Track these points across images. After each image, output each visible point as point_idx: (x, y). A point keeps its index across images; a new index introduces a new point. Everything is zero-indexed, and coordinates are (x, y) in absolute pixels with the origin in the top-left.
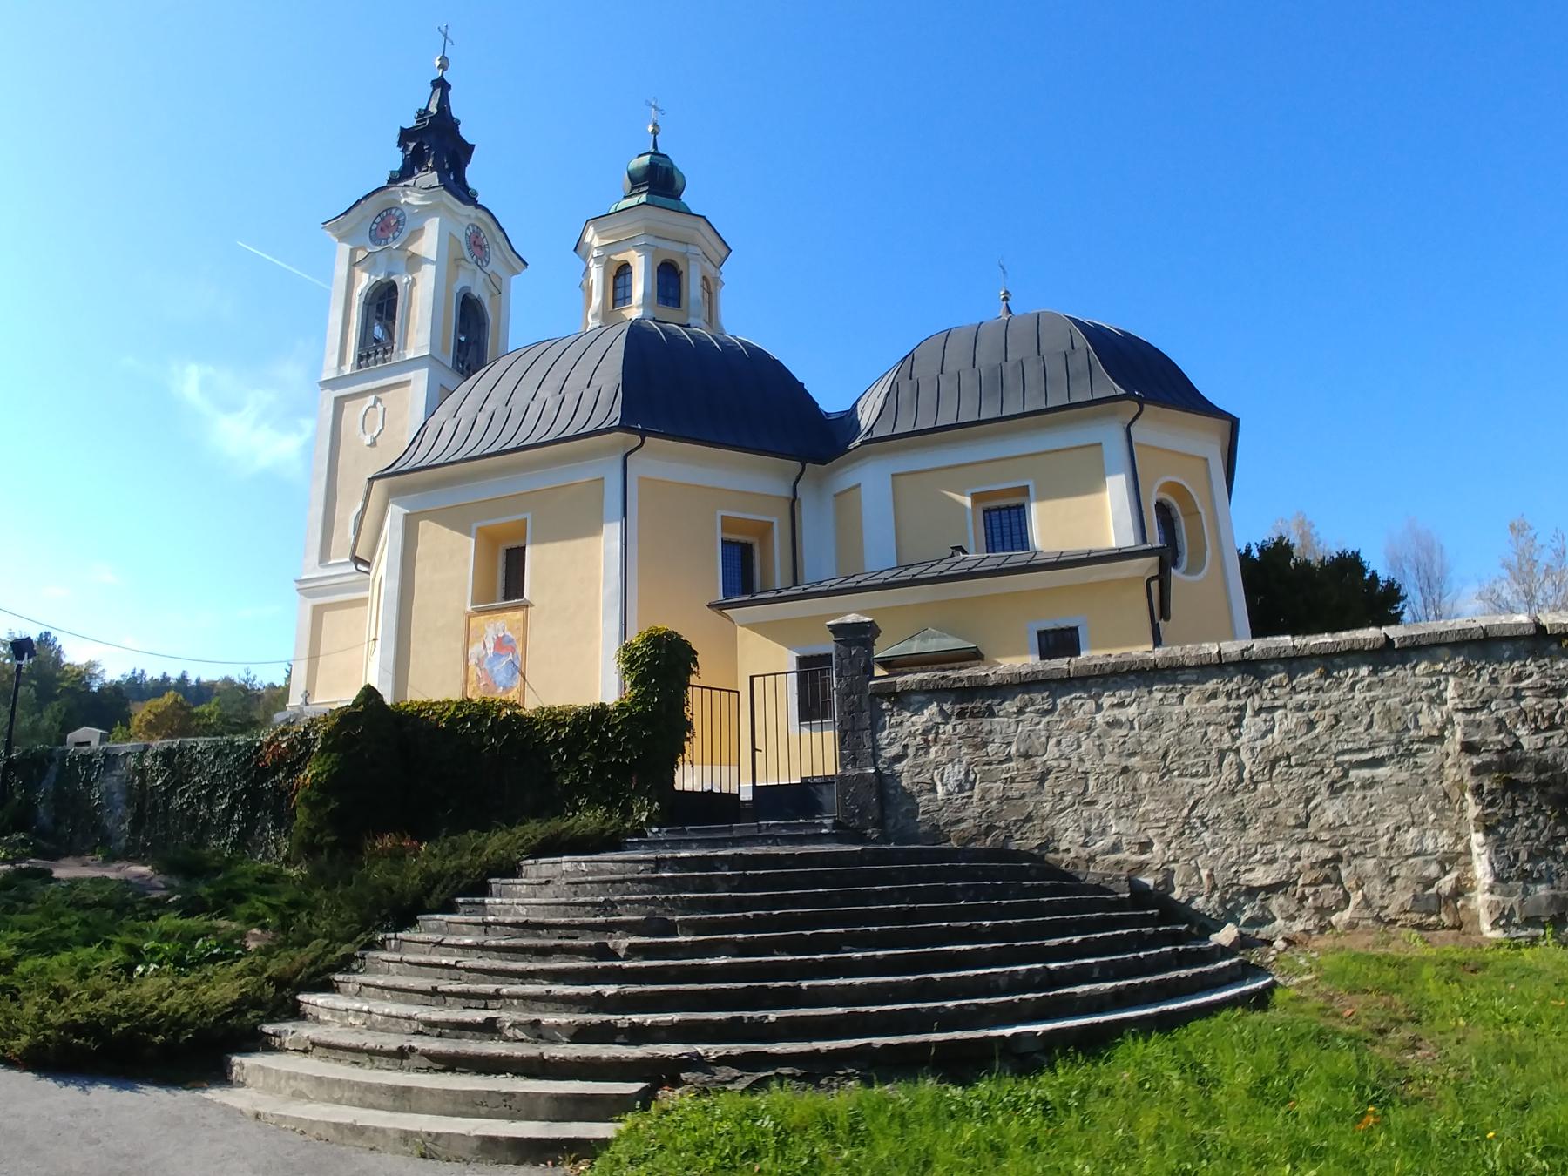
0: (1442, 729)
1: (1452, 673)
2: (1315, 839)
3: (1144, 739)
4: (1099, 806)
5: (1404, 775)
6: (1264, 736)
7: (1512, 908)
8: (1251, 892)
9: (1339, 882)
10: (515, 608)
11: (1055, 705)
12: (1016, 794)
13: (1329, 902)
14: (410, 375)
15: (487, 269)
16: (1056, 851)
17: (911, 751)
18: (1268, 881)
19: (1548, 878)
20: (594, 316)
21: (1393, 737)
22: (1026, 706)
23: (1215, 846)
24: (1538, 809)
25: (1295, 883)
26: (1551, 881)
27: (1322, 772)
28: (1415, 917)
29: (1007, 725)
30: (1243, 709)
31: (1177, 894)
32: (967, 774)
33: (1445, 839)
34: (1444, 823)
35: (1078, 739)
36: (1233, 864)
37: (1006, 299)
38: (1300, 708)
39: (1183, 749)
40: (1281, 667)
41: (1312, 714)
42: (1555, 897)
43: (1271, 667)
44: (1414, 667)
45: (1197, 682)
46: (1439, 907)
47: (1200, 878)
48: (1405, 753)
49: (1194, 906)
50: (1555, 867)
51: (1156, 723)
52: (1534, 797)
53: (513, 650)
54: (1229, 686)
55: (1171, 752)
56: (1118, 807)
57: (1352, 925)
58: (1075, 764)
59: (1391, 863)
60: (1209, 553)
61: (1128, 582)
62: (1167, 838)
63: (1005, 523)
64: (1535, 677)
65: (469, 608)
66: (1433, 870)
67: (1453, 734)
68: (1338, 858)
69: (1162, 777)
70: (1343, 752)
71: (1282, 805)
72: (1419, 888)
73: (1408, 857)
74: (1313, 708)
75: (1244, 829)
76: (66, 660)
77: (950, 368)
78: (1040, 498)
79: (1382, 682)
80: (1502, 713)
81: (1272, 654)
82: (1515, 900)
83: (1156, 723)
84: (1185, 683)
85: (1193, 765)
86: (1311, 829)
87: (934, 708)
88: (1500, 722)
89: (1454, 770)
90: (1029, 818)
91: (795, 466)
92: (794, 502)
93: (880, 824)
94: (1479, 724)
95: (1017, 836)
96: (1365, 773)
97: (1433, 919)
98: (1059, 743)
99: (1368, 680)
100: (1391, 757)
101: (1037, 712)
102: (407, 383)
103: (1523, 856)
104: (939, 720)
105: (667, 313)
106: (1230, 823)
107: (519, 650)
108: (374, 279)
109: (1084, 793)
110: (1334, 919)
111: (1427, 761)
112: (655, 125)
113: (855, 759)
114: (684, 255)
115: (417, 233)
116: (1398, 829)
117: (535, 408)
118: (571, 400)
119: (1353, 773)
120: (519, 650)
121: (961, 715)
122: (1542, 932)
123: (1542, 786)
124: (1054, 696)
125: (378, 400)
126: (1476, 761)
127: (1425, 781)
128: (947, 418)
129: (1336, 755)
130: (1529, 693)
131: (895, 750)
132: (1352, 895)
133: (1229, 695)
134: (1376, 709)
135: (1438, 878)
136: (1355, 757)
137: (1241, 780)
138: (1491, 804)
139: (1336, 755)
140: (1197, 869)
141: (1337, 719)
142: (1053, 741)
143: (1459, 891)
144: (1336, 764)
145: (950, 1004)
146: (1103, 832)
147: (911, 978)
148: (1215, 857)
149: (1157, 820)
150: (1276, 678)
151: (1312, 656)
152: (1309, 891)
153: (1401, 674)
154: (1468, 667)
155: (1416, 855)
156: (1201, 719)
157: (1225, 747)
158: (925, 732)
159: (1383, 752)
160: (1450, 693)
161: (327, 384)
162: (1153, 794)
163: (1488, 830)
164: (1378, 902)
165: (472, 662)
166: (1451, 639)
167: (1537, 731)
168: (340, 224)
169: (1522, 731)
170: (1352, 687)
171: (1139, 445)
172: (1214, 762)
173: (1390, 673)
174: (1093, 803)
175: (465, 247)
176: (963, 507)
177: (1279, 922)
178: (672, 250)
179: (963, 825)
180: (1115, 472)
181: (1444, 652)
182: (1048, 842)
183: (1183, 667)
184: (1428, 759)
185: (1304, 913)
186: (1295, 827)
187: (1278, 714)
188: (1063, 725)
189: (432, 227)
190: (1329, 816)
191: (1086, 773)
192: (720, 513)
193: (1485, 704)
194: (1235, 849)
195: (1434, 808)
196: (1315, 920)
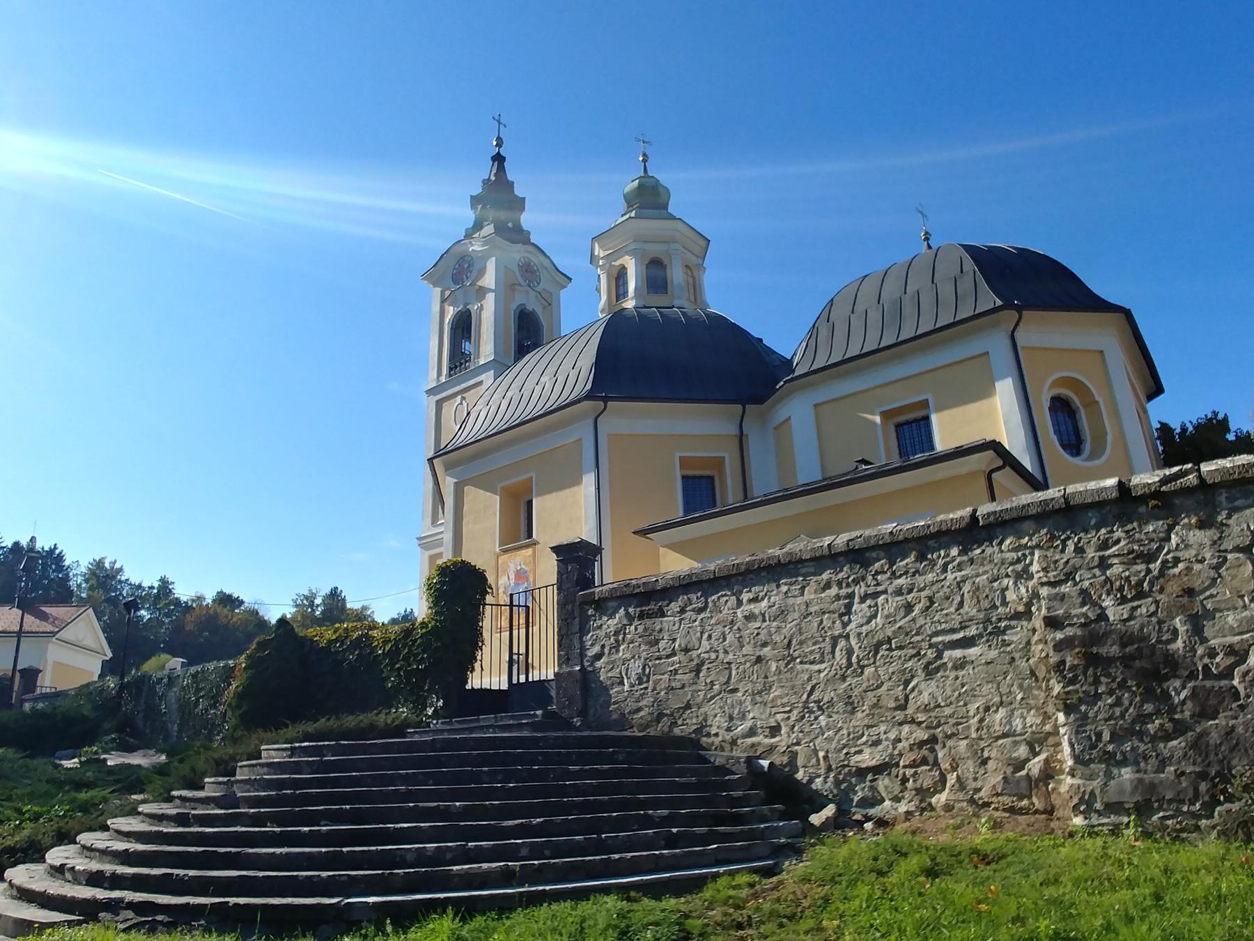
0: (1029, 605)
1: (1038, 546)
2: (913, 721)
3: (773, 630)
4: (739, 694)
5: (993, 654)
6: (868, 622)
7: (1092, 793)
8: (861, 773)
9: (936, 763)
10: (527, 546)
11: (706, 602)
12: (678, 685)
13: (927, 783)
14: (483, 377)
15: (539, 289)
16: (708, 735)
17: (606, 650)
18: (873, 763)
19: (1133, 760)
20: (602, 311)
21: (981, 616)
22: (686, 606)
23: (829, 729)
24: (1123, 685)
25: (897, 765)
26: (1137, 763)
27: (918, 653)
28: (1006, 800)
29: (675, 624)
30: (851, 596)
31: (800, 775)
32: (644, 669)
33: (1032, 719)
34: (1032, 702)
35: (723, 634)
36: (845, 746)
37: (927, 239)
38: (899, 592)
39: (803, 637)
40: (882, 554)
41: (909, 598)
42: (1140, 781)
43: (874, 555)
44: (1001, 543)
45: (815, 574)
46: (1027, 788)
47: (818, 760)
48: (994, 631)
49: (813, 786)
50: (1142, 747)
51: (782, 613)
52: (1118, 672)
53: (527, 580)
54: (840, 576)
55: (794, 642)
56: (753, 694)
57: (948, 808)
58: (721, 656)
59: (983, 744)
60: (1110, 438)
61: (971, 476)
62: (791, 722)
63: (912, 432)
64: (1123, 543)
66: (1023, 751)
67: (1039, 609)
68: (933, 740)
69: (787, 665)
70: (937, 634)
71: (884, 688)
72: (1009, 770)
73: (998, 738)
74: (910, 591)
75: (853, 712)
76: (349, 606)
77: (860, 307)
78: (938, 410)
79: (972, 561)
80: (1086, 584)
81: (873, 542)
82: (1096, 784)
83: (782, 613)
84: (805, 576)
85: (811, 652)
86: (910, 711)
87: (622, 611)
88: (1084, 593)
89: (1040, 647)
90: (688, 706)
92: (741, 437)
93: (583, 713)
94: (1062, 598)
95: (680, 722)
96: (958, 653)
97: (1025, 802)
98: (710, 637)
99: (958, 560)
100: (980, 636)
101: (693, 610)
102: (481, 383)
103: (1106, 736)
104: (625, 622)
105: (660, 300)
106: (840, 706)
107: (531, 579)
108: (457, 310)
109: (728, 682)
110: (933, 800)
111: (1015, 639)
112: (644, 155)
113: (568, 659)
115: (482, 272)
116: (987, 709)
117: (538, 389)
118: (561, 380)
119: (947, 654)
120: (531, 579)
121: (641, 617)
122: (1126, 820)
123: (1126, 660)
124: (706, 595)
125: (463, 398)
126: (1059, 635)
127: (1013, 659)
128: (854, 351)
129: (931, 636)
130: (1116, 561)
131: (596, 649)
132: (948, 776)
133: (839, 584)
134: (966, 588)
135: (1028, 760)
136: (948, 638)
137: (850, 665)
138: (1072, 681)
139: (931, 636)
140: (816, 752)
141: (931, 600)
142: (705, 636)
143: (1049, 773)
144: (931, 646)
145: (324, 874)
146: (743, 717)
147: (324, 850)
148: (829, 740)
149: (783, 705)
150: (877, 565)
151: (906, 540)
152: (909, 772)
153: (989, 551)
154: (1053, 538)
155: (1005, 735)
156: (817, 608)
157: (837, 633)
158: (616, 633)
159: (972, 631)
160: (1035, 568)
161: (430, 392)
162: (780, 681)
163: (1068, 709)
164: (972, 785)
166: (1032, 511)
167: (1123, 600)
168: (432, 276)
169: (1108, 602)
170: (945, 569)
171: (1023, 348)
172: (828, 649)
173: (978, 551)
174: (735, 690)
175: (518, 274)
176: (874, 423)
177: (887, 803)
178: (655, 250)
179: (642, 713)
180: (1004, 377)
181: (1028, 526)
182: (703, 727)
183: (801, 561)
184: (1015, 636)
185: (907, 795)
186: (896, 709)
187: (881, 599)
188: (713, 621)
190: (925, 698)
191: (729, 663)
192: (678, 455)
193: (1069, 576)
194: (845, 732)
195: (1021, 686)
196: (916, 802)
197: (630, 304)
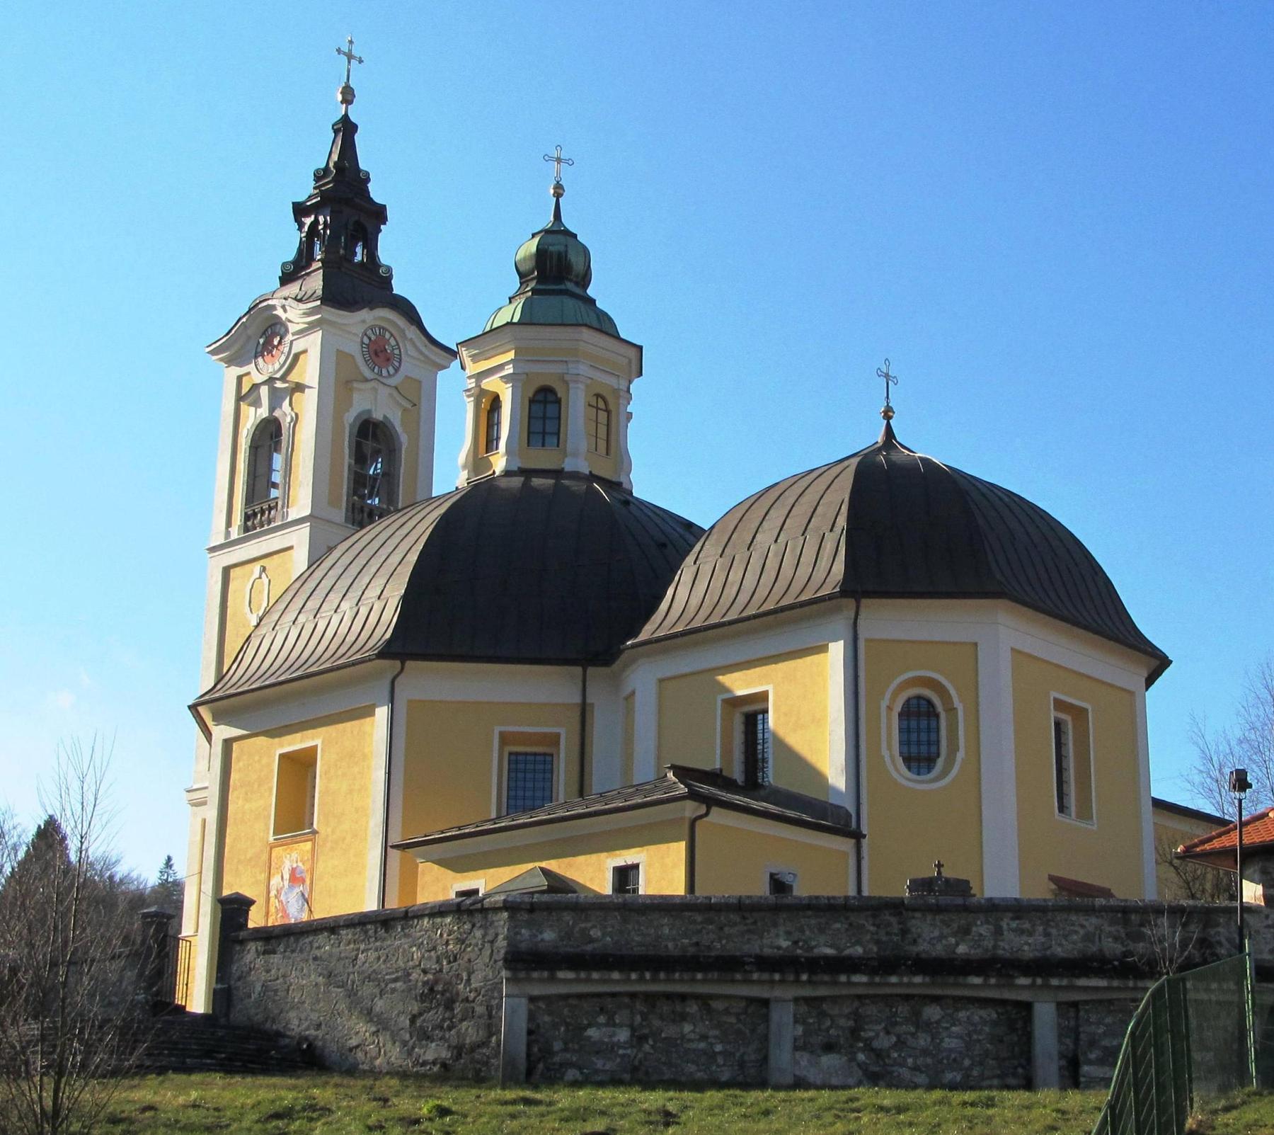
53: (303, 881)
65: (271, 839)
91: (578, 670)
92: (584, 711)
114: (562, 378)
118: (364, 611)
120: (308, 882)
125: (264, 569)
165: (273, 893)
178: (546, 373)
183: (394, 919)
189: (313, 343)
197: (499, 463)
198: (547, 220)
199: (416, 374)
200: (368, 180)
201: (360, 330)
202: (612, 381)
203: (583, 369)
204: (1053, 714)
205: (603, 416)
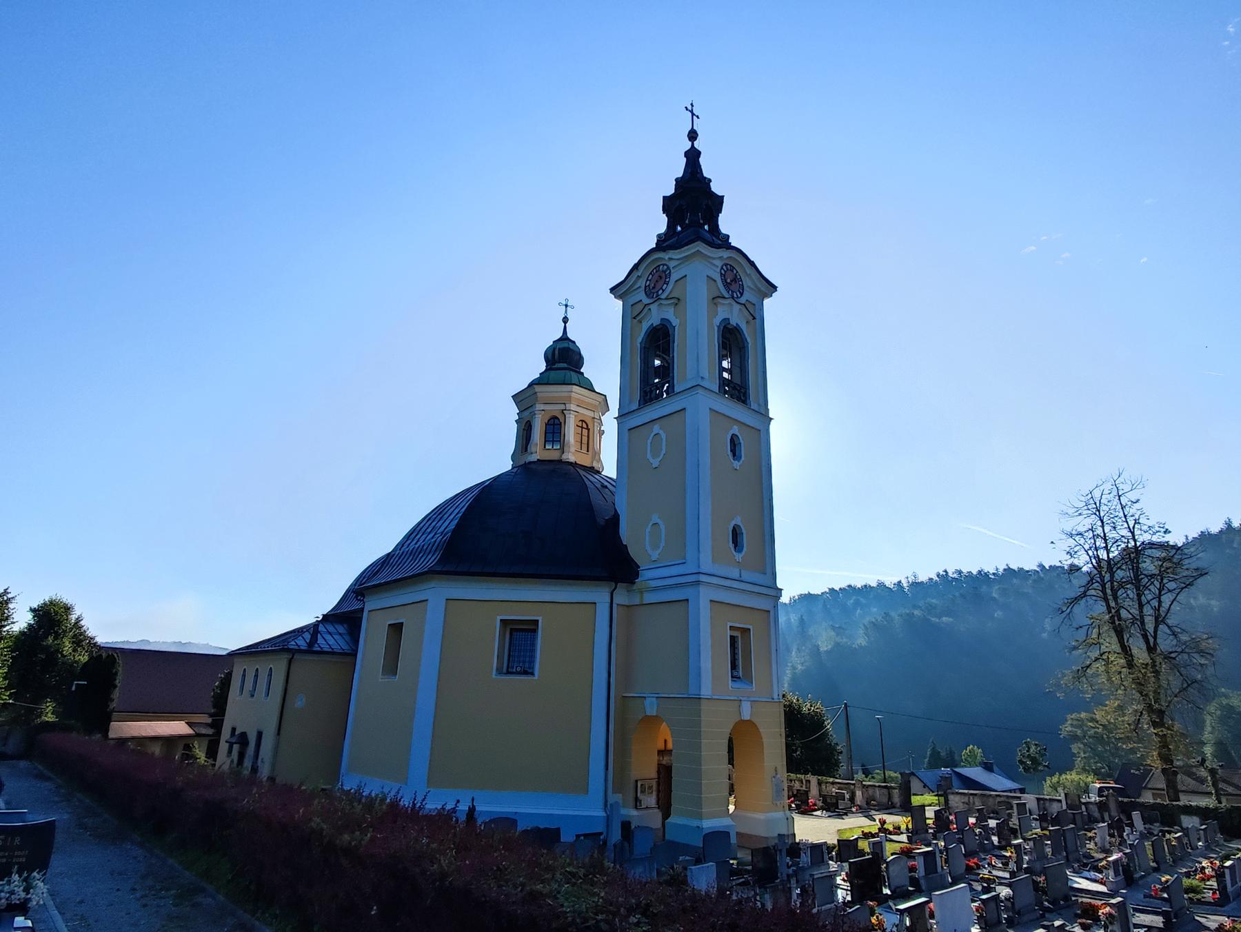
198: (559, 335)
199: (753, 300)
200: (710, 180)
201: (719, 263)
202: (591, 414)
203: (573, 407)
204: (729, 633)
205: (585, 432)
